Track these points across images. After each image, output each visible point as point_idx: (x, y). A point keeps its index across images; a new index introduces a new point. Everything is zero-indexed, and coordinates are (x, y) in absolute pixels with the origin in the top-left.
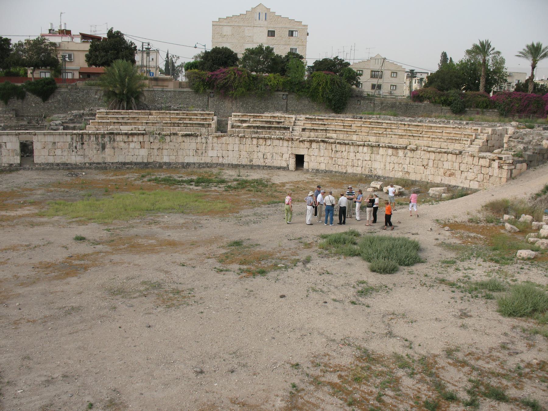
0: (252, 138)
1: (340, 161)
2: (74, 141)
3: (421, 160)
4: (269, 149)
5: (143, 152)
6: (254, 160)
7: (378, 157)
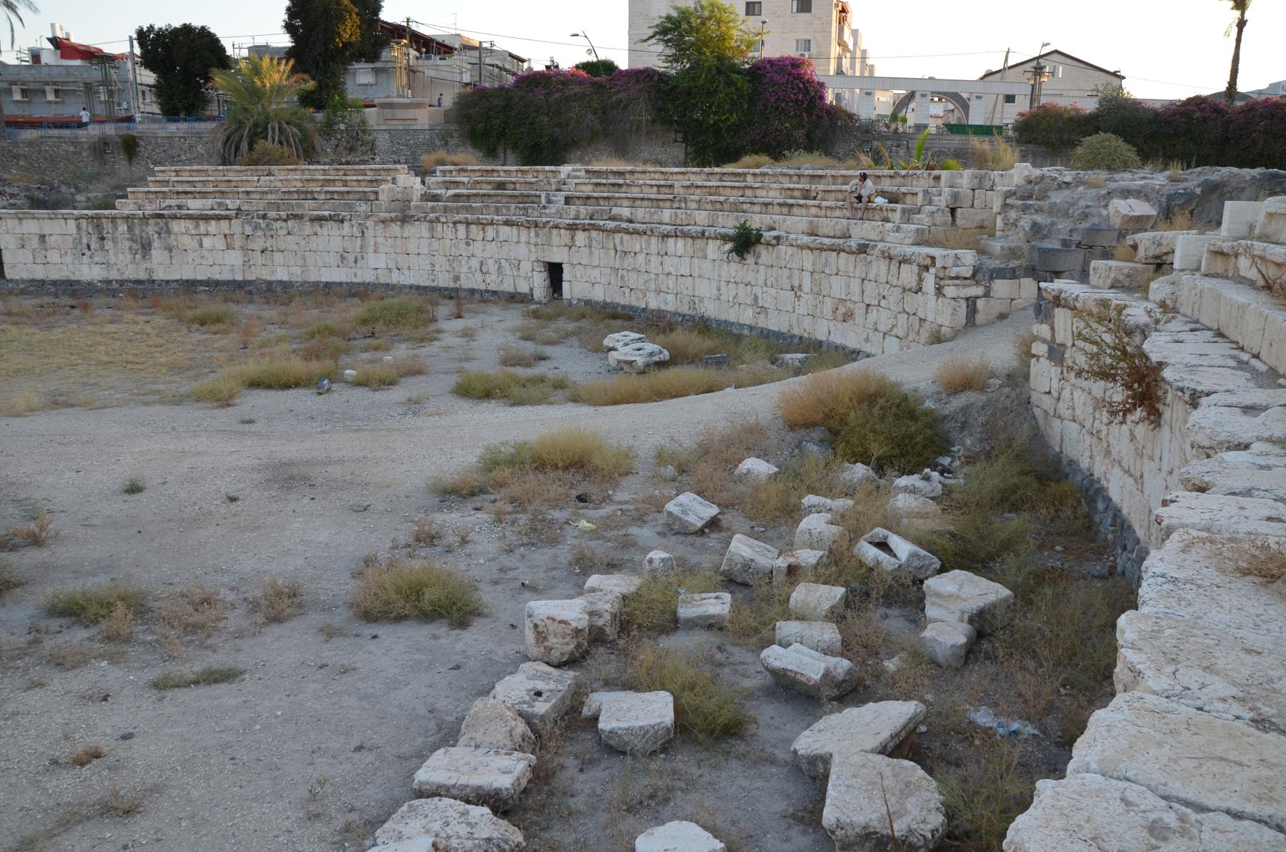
0: (455, 223)
1: (633, 280)
2: (83, 234)
4: (492, 248)
5: (235, 258)
6: (463, 276)
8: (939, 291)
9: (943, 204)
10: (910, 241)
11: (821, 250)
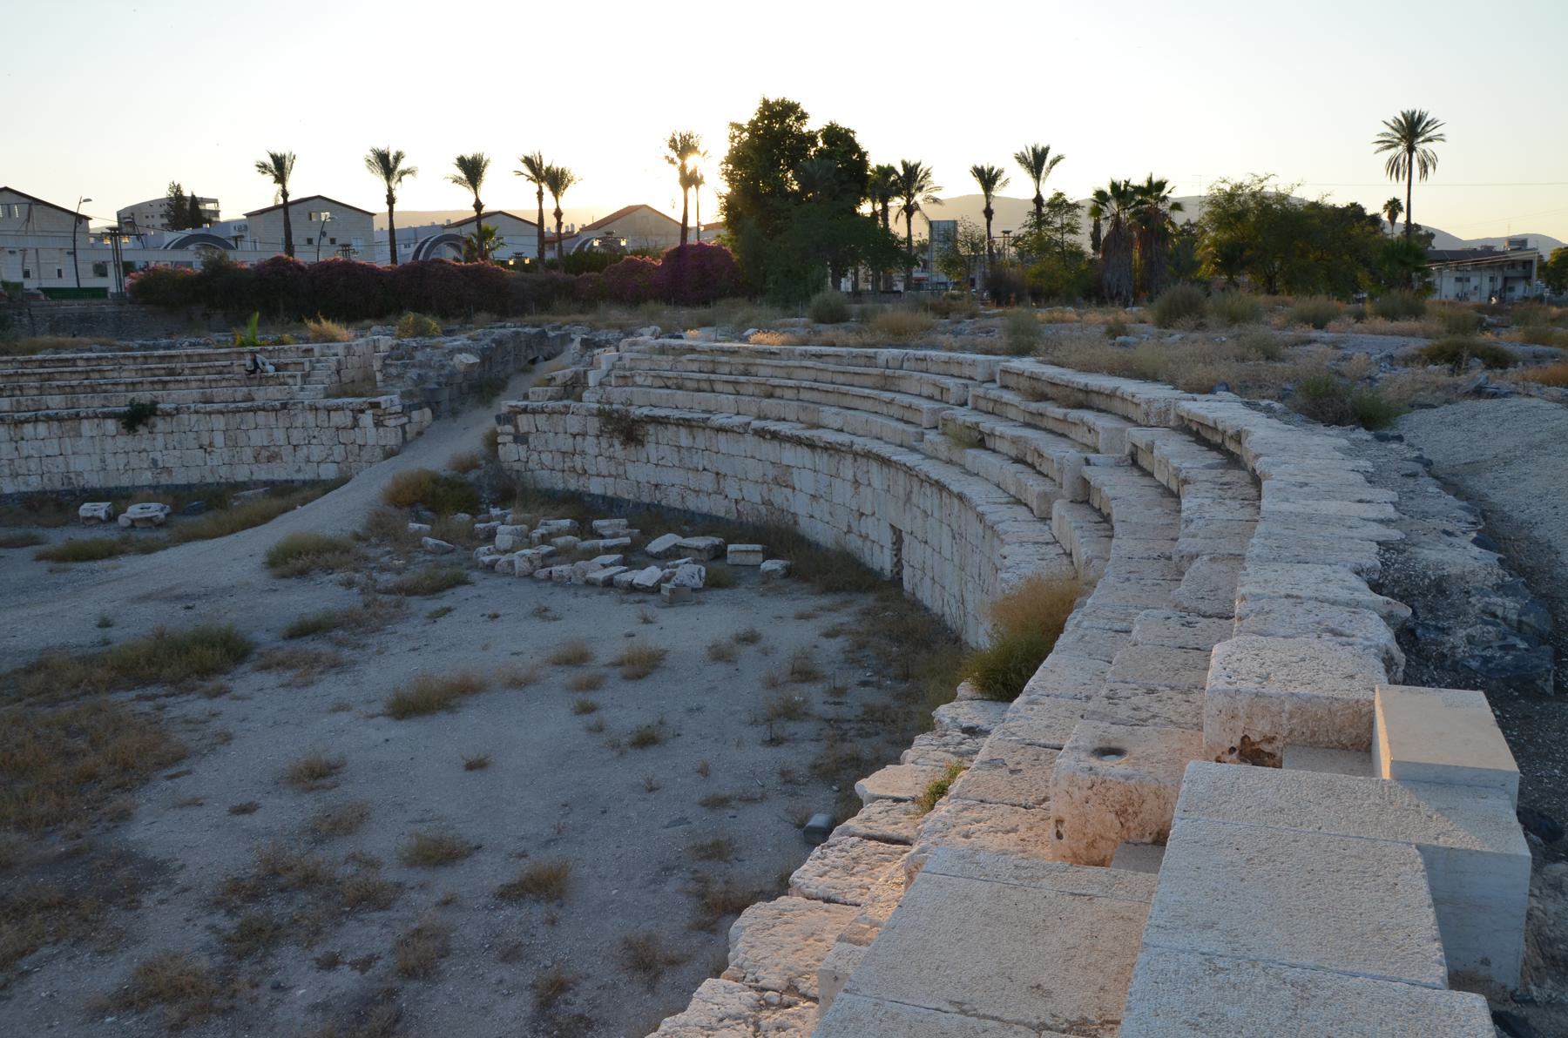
3: (192, 435)
7: (82, 444)
8: (378, 424)
11: (234, 412)
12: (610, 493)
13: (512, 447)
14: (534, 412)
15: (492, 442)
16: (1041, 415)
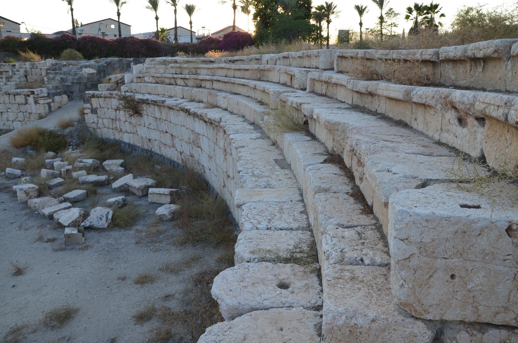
8: (36, 102)
9: (22, 74)
10: (14, 88)
12: (132, 143)
13: (90, 115)
14: (98, 97)
15: (83, 114)
16: (371, 94)
